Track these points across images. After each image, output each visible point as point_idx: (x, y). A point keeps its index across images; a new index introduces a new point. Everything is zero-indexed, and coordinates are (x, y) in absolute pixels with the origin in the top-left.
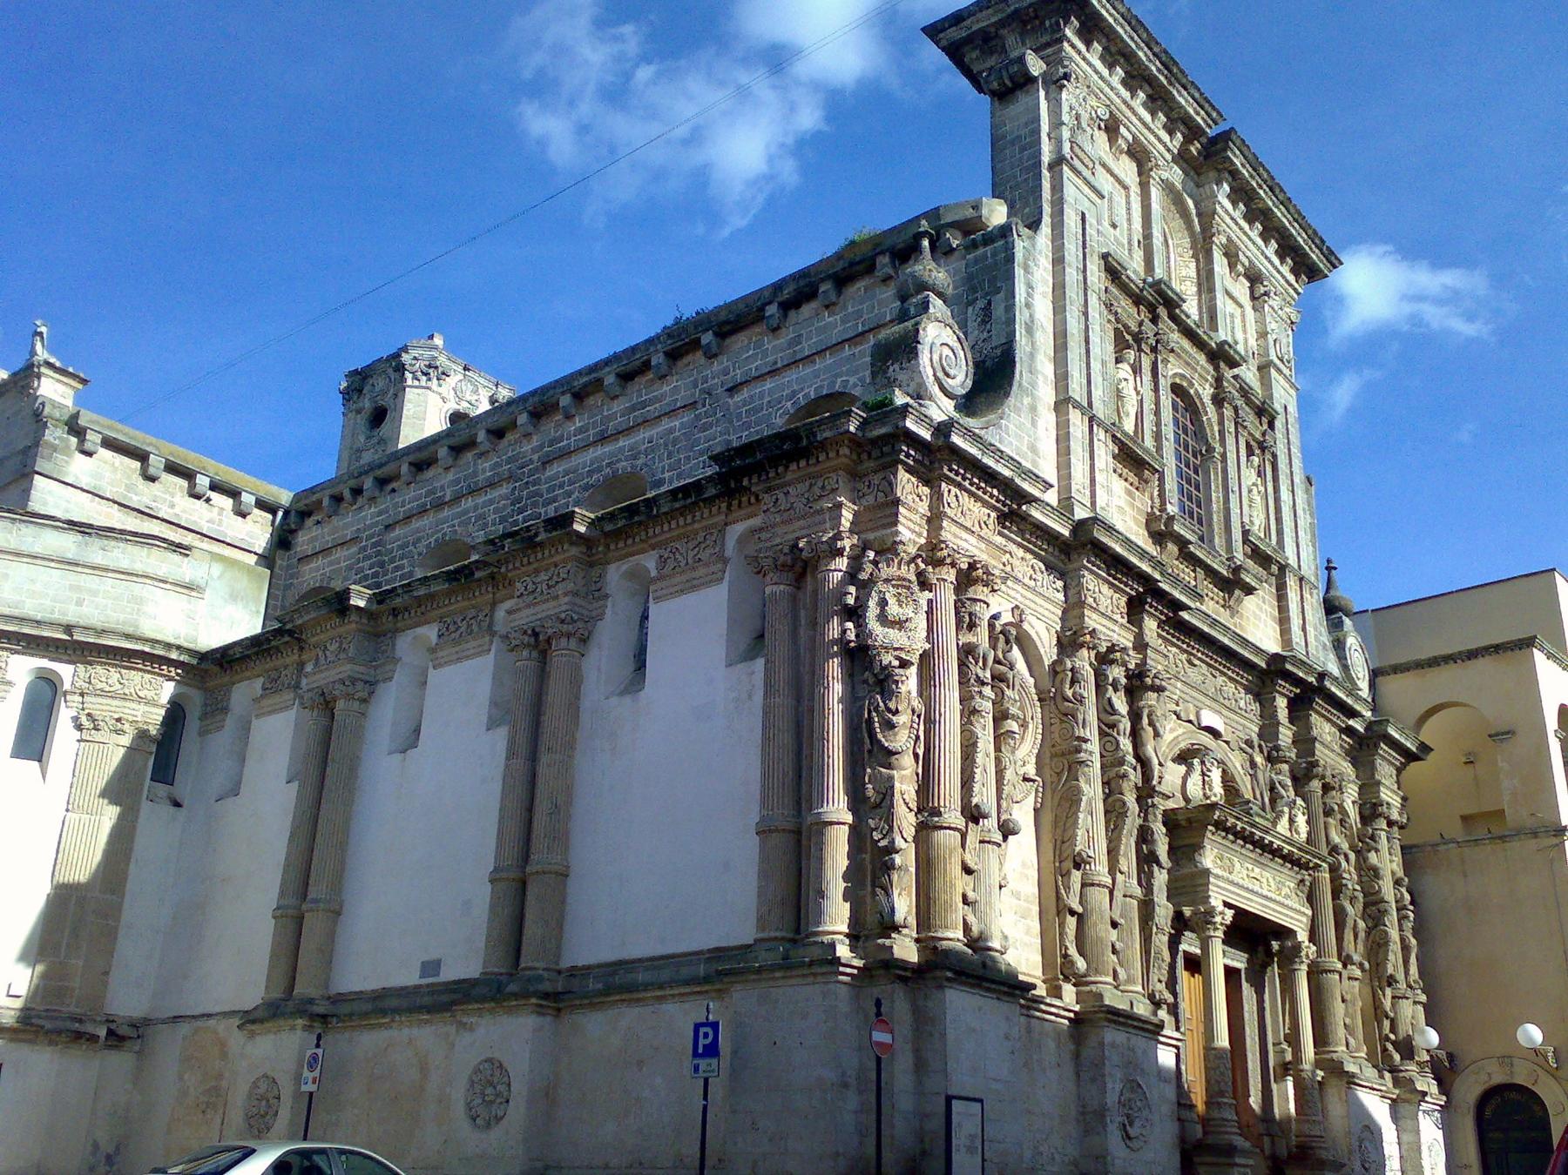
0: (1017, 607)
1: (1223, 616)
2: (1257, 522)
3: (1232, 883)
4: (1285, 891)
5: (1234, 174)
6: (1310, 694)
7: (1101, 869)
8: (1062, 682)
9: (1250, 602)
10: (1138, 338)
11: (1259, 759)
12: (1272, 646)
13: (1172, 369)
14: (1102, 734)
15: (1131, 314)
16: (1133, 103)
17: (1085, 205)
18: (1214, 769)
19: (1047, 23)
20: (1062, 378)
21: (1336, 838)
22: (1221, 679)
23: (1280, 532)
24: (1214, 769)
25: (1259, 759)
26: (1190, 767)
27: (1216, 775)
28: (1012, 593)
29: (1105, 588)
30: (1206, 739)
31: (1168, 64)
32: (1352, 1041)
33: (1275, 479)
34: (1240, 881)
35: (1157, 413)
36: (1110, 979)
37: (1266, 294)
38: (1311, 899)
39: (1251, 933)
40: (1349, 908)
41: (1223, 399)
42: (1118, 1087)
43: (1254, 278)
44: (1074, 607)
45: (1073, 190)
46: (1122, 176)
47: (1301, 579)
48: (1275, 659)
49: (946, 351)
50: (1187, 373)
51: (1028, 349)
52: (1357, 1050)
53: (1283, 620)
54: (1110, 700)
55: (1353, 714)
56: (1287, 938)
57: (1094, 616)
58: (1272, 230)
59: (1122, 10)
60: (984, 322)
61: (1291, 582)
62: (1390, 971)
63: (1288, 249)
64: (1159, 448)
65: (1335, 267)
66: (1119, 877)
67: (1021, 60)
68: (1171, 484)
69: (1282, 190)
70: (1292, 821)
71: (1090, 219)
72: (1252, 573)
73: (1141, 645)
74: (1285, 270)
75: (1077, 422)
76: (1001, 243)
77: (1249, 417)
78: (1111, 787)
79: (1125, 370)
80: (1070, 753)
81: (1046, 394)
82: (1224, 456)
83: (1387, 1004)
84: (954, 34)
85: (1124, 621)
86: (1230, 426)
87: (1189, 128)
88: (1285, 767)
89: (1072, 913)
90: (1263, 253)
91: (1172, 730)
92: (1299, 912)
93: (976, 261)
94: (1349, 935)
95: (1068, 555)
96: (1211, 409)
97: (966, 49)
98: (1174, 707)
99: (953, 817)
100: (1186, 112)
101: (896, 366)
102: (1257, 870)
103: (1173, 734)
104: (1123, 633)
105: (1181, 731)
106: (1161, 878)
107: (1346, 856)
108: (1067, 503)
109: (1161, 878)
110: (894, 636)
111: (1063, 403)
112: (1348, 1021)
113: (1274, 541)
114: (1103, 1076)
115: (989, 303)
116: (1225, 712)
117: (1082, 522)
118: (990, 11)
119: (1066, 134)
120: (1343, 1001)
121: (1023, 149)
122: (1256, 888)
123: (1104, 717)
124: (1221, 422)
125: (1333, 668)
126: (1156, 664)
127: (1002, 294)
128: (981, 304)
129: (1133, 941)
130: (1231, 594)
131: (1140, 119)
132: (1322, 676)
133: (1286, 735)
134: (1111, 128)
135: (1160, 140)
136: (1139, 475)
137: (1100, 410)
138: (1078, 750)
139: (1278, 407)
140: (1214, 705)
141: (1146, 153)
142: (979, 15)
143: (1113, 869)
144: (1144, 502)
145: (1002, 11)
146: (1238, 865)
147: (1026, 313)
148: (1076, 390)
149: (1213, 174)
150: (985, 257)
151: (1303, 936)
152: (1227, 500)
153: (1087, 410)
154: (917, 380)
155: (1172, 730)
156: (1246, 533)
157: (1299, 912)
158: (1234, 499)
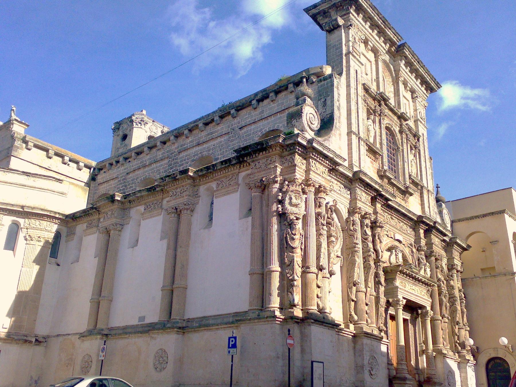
1: (403, 203)
4: (423, 293)
5: (406, 57)
8: (350, 225)
11: (414, 250)
13: (386, 122)
14: (363, 242)
18: (399, 253)
22: (402, 224)
23: (421, 175)
24: (399, 253)
25: (414, 250)
27: (400, 255)
29: (364, 194)
30: (397, 244)
32: (445, 343)
35: (381, 136)
36: (365, 322)
38: (431, 296)
40: (444, 299)
41: (403, 132)
42: (368, 358)
43: (413, 92)
44: (353, 200)
47: (428, 191)
48: (420, 217)
50: (391, 123)
53: (422, 204)
54: (365, 231)
55: (445, 235)
57: (360, 203)
58: (418, 76)
59: (369, 3)
60: (324, 106)
62: (457, 320)
63: (424, 82)
64: (381, 148)
68: (385, 160)
70: (425, 270)
71: (359, 72)
72: (412, 189)
73: (375, 213)
74: (423, 89)
76: (330, 80)
77: (411, 138)
78: (366, 259)
80: (352, 248)
83: (457, 330)
86: (405, 140)
88: (423, 253)
90: (416, 83)
93: (321, 86)
94: (444, 308)
96: (399, 135)
98: (386, 233)
99: (314, 269)
100: (390, 37)
101: (295, 121)
103: (386, 242)
106: (382, 289)
107: (443, 282)
108: (351, 166)
109: (382, 289)
115: (326, 100)
116: (403, 235)
122: (413, 292)
124: (402, 139)
126: (380, 219)
127: (330, 97)
128: (323, 100)
130: (405, 196)
132: (435, 223)
133: (423, 242)
134: (366, 42)
138: (355, 247)
141: (377, 50)
143: (366, 286)
144: (376, 165)
146: (407, 285)
149: (399, 57)
151: (429, 308)
155: (386, 240)
156: (410, 176)
158: (406, 164)
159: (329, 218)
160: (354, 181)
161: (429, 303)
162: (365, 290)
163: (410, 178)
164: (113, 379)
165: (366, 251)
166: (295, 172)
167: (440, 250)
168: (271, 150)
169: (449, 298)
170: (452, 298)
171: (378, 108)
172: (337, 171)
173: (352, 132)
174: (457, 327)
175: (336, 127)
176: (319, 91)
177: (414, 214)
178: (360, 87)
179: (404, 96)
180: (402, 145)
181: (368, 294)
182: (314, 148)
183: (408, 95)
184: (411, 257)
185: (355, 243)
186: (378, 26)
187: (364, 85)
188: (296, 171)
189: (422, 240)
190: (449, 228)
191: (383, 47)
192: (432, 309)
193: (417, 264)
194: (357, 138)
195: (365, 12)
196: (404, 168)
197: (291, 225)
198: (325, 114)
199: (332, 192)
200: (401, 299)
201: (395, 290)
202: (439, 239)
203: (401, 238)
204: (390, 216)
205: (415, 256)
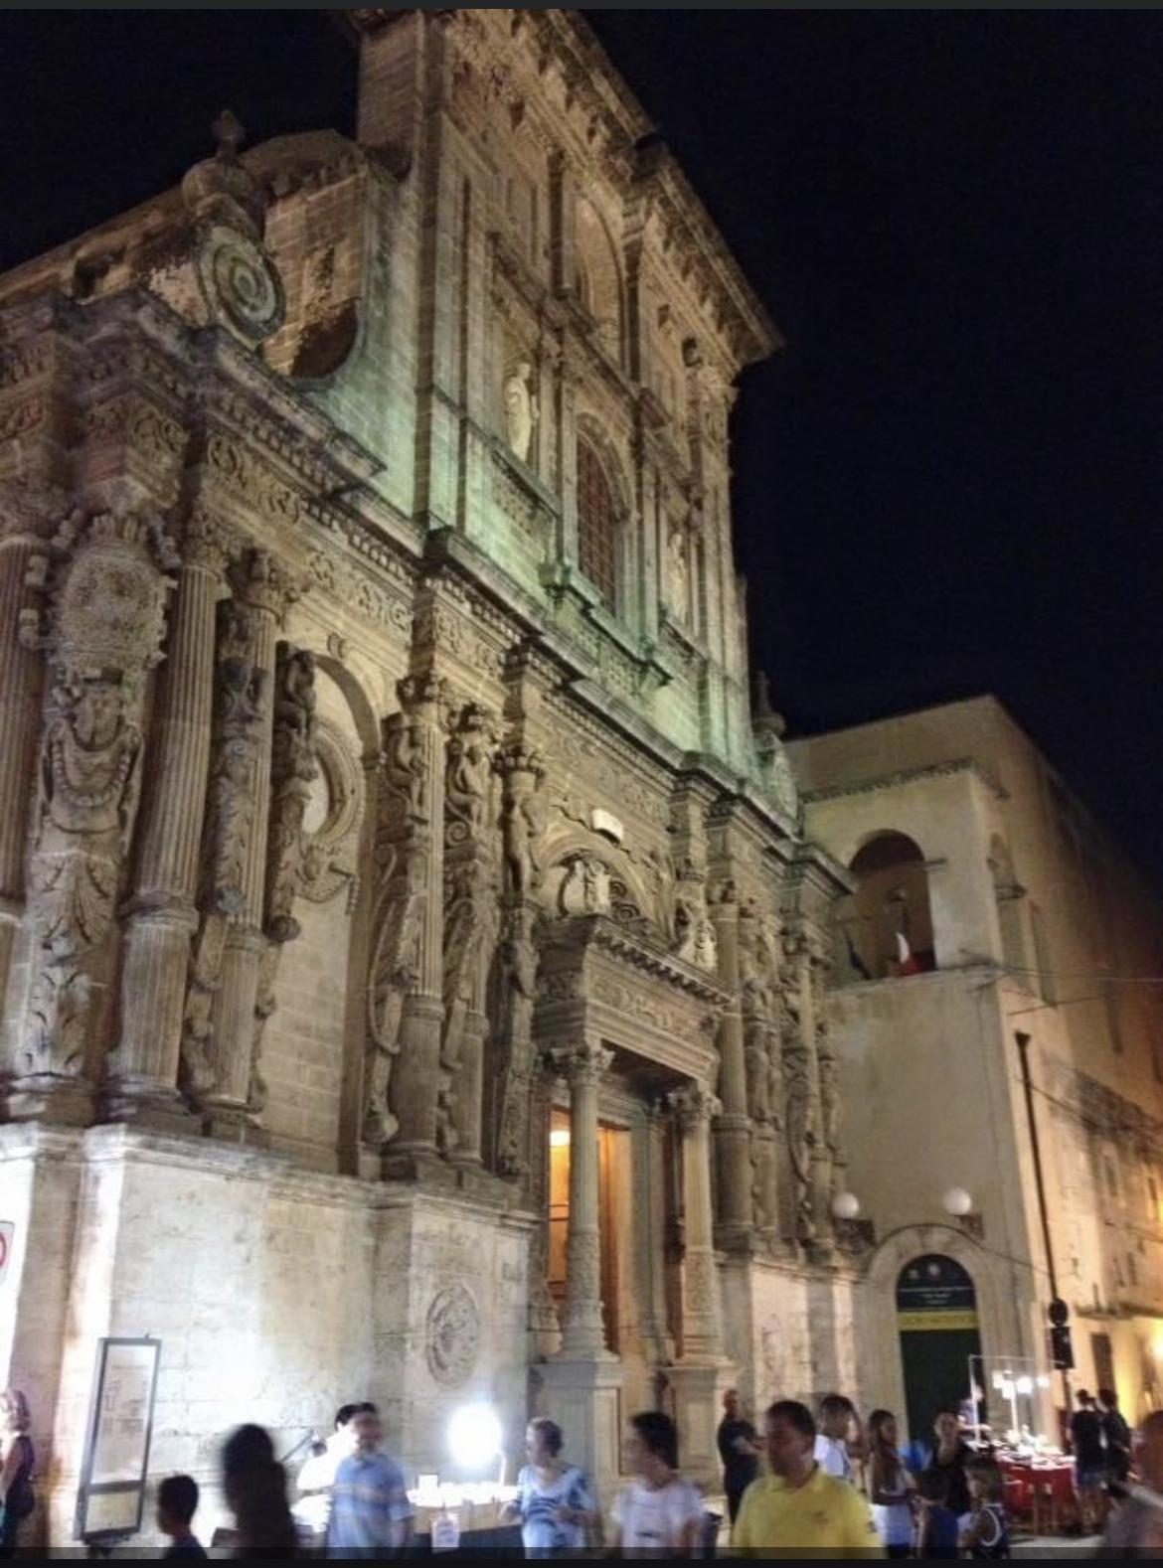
4: (685, 1031)
6: (725, 803)
8: (397, 743)
9: (665, 697)
11: (665, 876)
13: (581, 404)
14: (450, 818)
21: (751, 973)
23: (703, 624)
25: (665, 876)
26: (572, 870)
27: (602, 883)
30: (602, 845)
32: (761, 1214)
34: (623, 1014)
35: (558, 449)
36: (430, 1144)
37: (700, 360)
40: (763, 1056)
42: (429, 1295)
48: (691, 756)
52: (768, 1223)
54: (463, 774)
55: (778, 833)
57: (449, 664)
60: (323, 277)
62: (809, 1127)
64: (559, 491)
68: (570, 537)
71: (478, 191)
73: (514, 712)
75: (444, 428)
78: (458, 895)
79: (518, 387)
82: (641, 523)
83: (804, 1165)
89: (384, 1052)
91: (557, 829)
94: (762, 1087)
98: (559, 801)
101: (162, 274)
103: (554, 833)
104: (490, 692)
105: (567, 832)
106: (524, 1010)
107: (763, 996)
108: (422, 516)
109: (524, 1010)
111: (426, 390)
112: (757, 1190)
114: (406, 1281)
115: (331, 253)
117: (437, 532)
120: (752, 1163)
122: (649, 1026)
123: (457, 795)
124: (640, 485)
126: (535, 740)
128: (320, 255)
129: (471, 1090)
132: (741, 782)
133: (698, 850)
137: (476, 411)
139: (707, 485)
144: (541, 552)
151: (705, 1087)
152: (641, 572)
153: (461, 408)
155: (557, 829)
156: (663, 612)
158: (650, 572)
161: (707, 1066)
162: (440, 1009)
164: (472, 1301)
165: (460, 855)
168: (19, 372)
175: (362, 355)
176: (310, 223)
180: (640, 508)
189: (693, 841)
190: (792, 811)
194: (457, 424)
196: (642, 584)
198: (325, 305)
200: (595, 1046)
201: (575, 1015)
203: (618, 831)
205: (665, 895)
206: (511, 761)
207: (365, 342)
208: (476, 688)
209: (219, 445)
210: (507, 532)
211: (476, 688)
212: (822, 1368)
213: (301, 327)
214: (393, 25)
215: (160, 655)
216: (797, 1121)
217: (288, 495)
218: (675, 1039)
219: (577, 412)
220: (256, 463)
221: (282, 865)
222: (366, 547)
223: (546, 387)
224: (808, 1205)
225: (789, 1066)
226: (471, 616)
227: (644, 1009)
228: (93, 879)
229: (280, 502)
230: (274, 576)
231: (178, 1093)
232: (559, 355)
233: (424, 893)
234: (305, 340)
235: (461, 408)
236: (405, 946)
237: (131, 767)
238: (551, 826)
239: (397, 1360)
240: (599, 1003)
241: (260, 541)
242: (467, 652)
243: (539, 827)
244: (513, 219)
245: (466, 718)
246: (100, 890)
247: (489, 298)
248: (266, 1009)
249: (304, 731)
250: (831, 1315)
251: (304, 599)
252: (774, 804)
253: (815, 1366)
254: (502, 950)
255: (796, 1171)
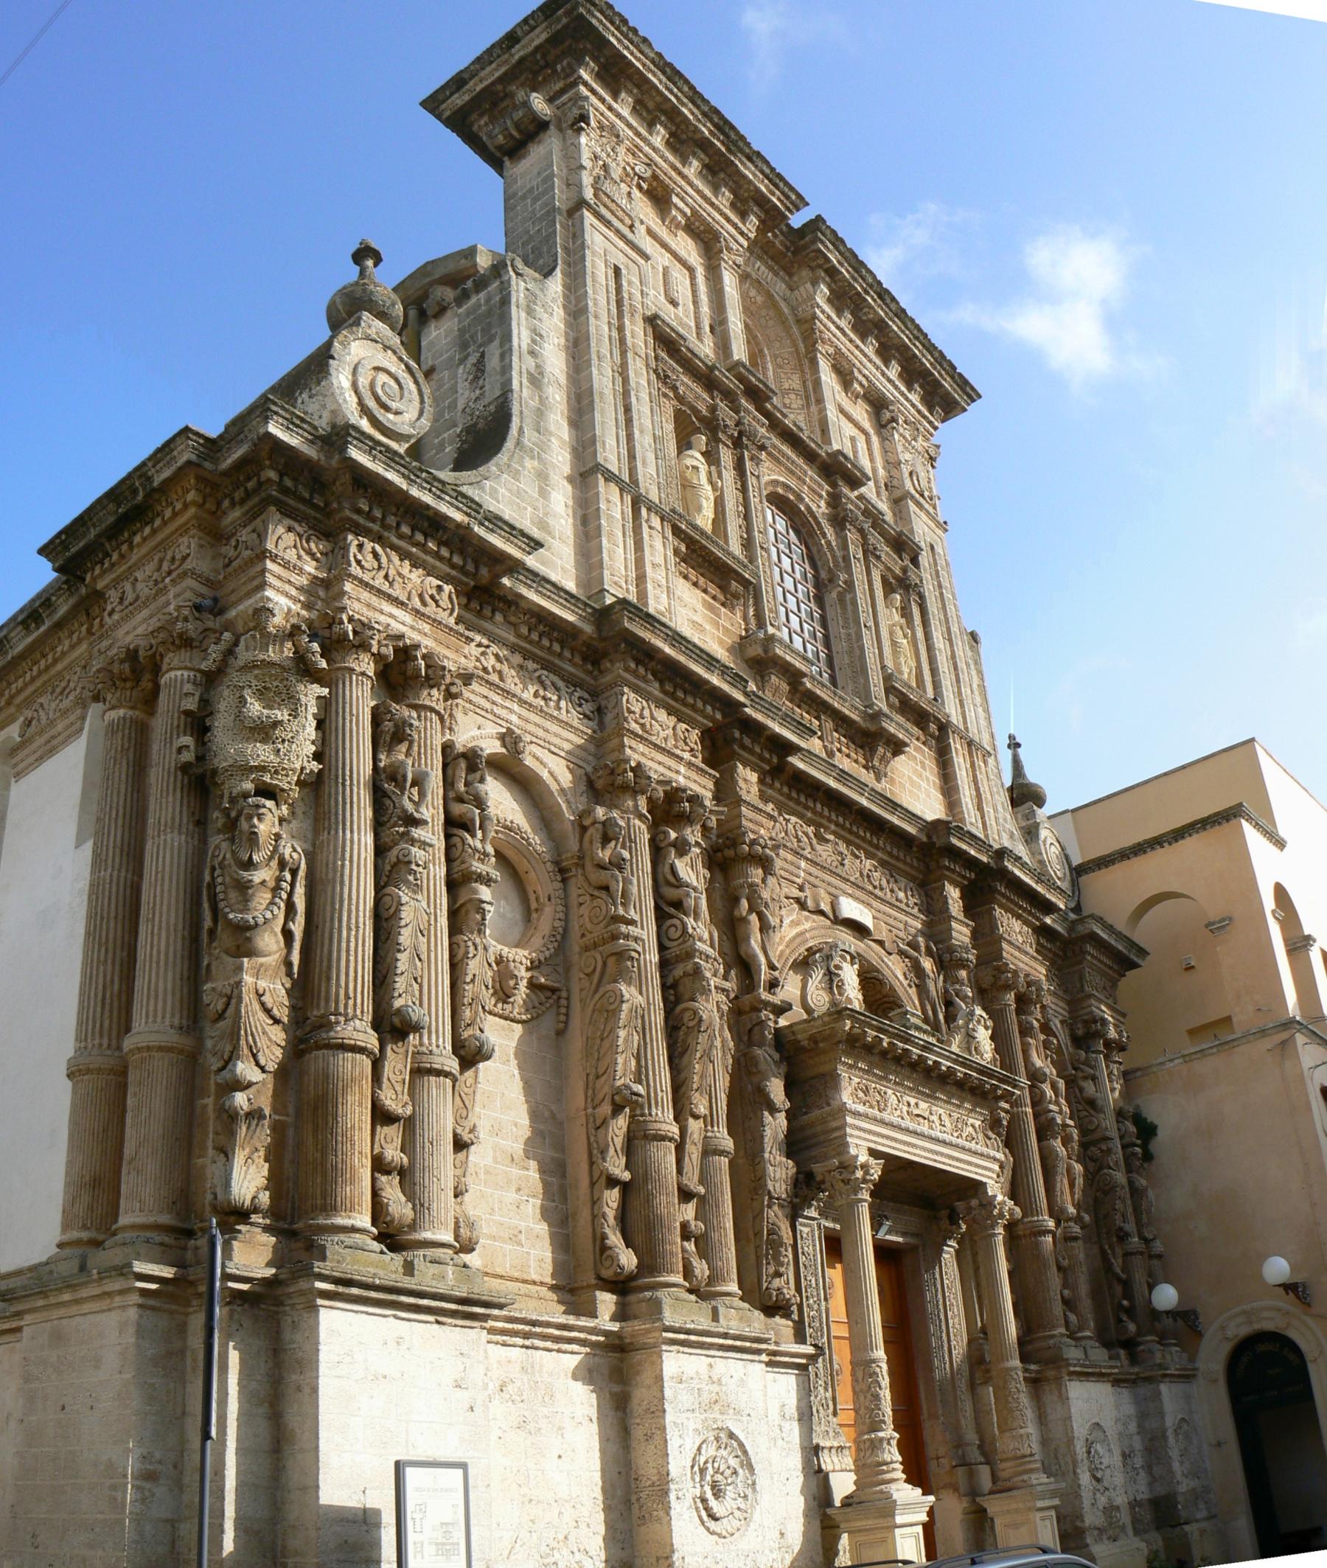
0: (510, 731)
1: (867, 777)
2: (906, 670)
3: (883, 1122)
5: (832, 272)
7: (664, 1120)
9: (901, 765)
10: (712, 426)
11: (927, 964)
12: (930, 807)
14: (661, 916)
15: (700, 398)
16: (685, 171)
17: (621, 261)
18: (846, 966)
19: (559, 67)
20: (584, 446)
22: (868, 864)
23: (937, 685)
24: (846, 966)
25: (927, 964)
27: (850, 975)
28: (503, 713)
29: (662, 715)
30: (847, 939)
31: (724, 126)
32: (1073, 1318)
33: (925, 623)
38: (1012, 1141)
39: (922, 1197)
41: (844, 519)
43: (877, 404)
45: (596, 238)
46: (683, 253)
47: (970, 743)
49: (383, 378)
50: (793, 483)
51: (534, 403)
52: (1081, 1329)
55: (1048, 907)
56: (975, 1195)
58: (889, 349)
59: (652, 55)
60: (476, 378)
61: (956, 745)
63: (913, 373)
65: (973, 401)
66: (694, 1126)
67: (526, 104)
69: (893, 299)
72: (896, 726)
74: (914, 398)
75: (613, 505)
76: (497, 284)
77: (885, 550)
79: (695, 458)
80: (604, 942)
81: (561, 460)
83: (1117, 1265)
84: (459, 100)
85: (698, 761)
87: (766, 212)
88: (963, 974)
90: (883, 374)
91: (794, 923)
92: (988, 1157)
93: (468, 314)
94: (1062, 1183)
95: (596, 663)
96: (829, 531)
97: (474, 116)
98: (796, 893)
99: (360, 1031)
100: (758, 190)
102: (923, 1105)
103: (791, 930)
105: (807, 925)
109: (775, 1126)
110: (262, 753)
113: (930, 694)
115: (483, 355)
116: (875, 904)
118: (494, 65)
119: (587, 179)
121: (536, 200)
122: (924, 1128)
125: (1021, 850)
127: (497, 342)
128: (473, 359)
130: (873, 751)
131: (698, 192)
132: (1001, 853)
133: (961, 933)
134: (659, 196)
135: (728, 220)
136: (723, 588)
138: (615, 937)
140: (858, 893)
141: (716, 236)
142: (482, 74)
143: (681, 1111)
145: (506, 61)
146: (893, 1100)
147: (530, 363)
148: (610, 454)
149: (805, 273)
150: (478, 305)
151: (996, 1189)
153: (630, 487)
154: (330, 406)
155: (794, 923)
157: (988, 1157)
159: (460, 800)
160: (597, 652)
162: (674, 1130)
163: (890, 689)
166: (263, 585)
167: (1033, 963)
169: (1084, 1145)
170: (1095, 1143)
171: (724, 410)
172: (511, 603)
173: (597, 468)
174: (1119, 1251)
175: (518, 443)
176: (462, 331)
177: (912, 817)
178: (638, 335)
179: (842, 411)
181: (693, 1152)
182: (363, 480)
183: (860, 412)
184: (913, 992)
185: (617, 919)
186: (704, 145)
187: (652, 321)
188: (270, 579)
190: (1065, 885)
191: (738, 233)
192: (1013, 1194)
193: (941, 1017)
194: (628, 499)
195: (641, 83)
197: (237, 828)
199: (475, 686)
200: (863, 1158)
202: (1026, 922)
203: (866, 918)
204: (810, 830)
206: (729, 853)
207: (521, 430)
208: (678, 772)
209: (360, 546)
210: (700, 607)
211: (678, 772)
212: (1156, 1470)
213: (458, 430)
214: (530, 145)
215: (315, 766)
216: (1106, 1216)
217: (439, 588)
218: (954, 1140)
219: (765, 479)
220: (401, 560)
221: (396, 994)
222: (535, 636)
223: (726, 456)
224: (1125, 1303)
225: (1091, 1159)
226: (661, 695)
227: (916, 1112)
228: (263, 1004)
229: (432, 597)
230: (430, 672)
231: (375, 1231)
232: (738, 423)
233: (640, 1000)
234: (463, 442)
235: (630, 487)
236: (624, 1065)
237: (292, 885)
238: (787, 921)
239: (661, 1513)
240: (861, 1108)
241: (412, 637)
242: (663, 734)
243: (773, 921)
244: (674, 303)
245: (670, 810)
246: (272, 1017)
247: (653, 377)
248: (466, 1137)
249: (479, 834)
250: (1161, 1414)
251: (466, 694)
252: (1041, 877)
253: (1149, 1468)
254: (742, 1059)
255: (1108, 1267)
